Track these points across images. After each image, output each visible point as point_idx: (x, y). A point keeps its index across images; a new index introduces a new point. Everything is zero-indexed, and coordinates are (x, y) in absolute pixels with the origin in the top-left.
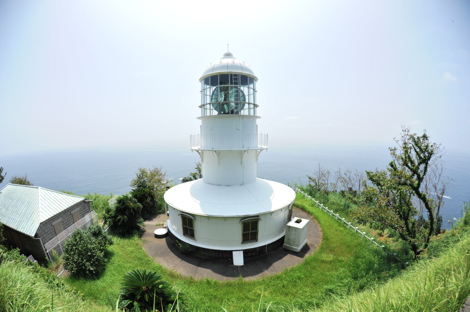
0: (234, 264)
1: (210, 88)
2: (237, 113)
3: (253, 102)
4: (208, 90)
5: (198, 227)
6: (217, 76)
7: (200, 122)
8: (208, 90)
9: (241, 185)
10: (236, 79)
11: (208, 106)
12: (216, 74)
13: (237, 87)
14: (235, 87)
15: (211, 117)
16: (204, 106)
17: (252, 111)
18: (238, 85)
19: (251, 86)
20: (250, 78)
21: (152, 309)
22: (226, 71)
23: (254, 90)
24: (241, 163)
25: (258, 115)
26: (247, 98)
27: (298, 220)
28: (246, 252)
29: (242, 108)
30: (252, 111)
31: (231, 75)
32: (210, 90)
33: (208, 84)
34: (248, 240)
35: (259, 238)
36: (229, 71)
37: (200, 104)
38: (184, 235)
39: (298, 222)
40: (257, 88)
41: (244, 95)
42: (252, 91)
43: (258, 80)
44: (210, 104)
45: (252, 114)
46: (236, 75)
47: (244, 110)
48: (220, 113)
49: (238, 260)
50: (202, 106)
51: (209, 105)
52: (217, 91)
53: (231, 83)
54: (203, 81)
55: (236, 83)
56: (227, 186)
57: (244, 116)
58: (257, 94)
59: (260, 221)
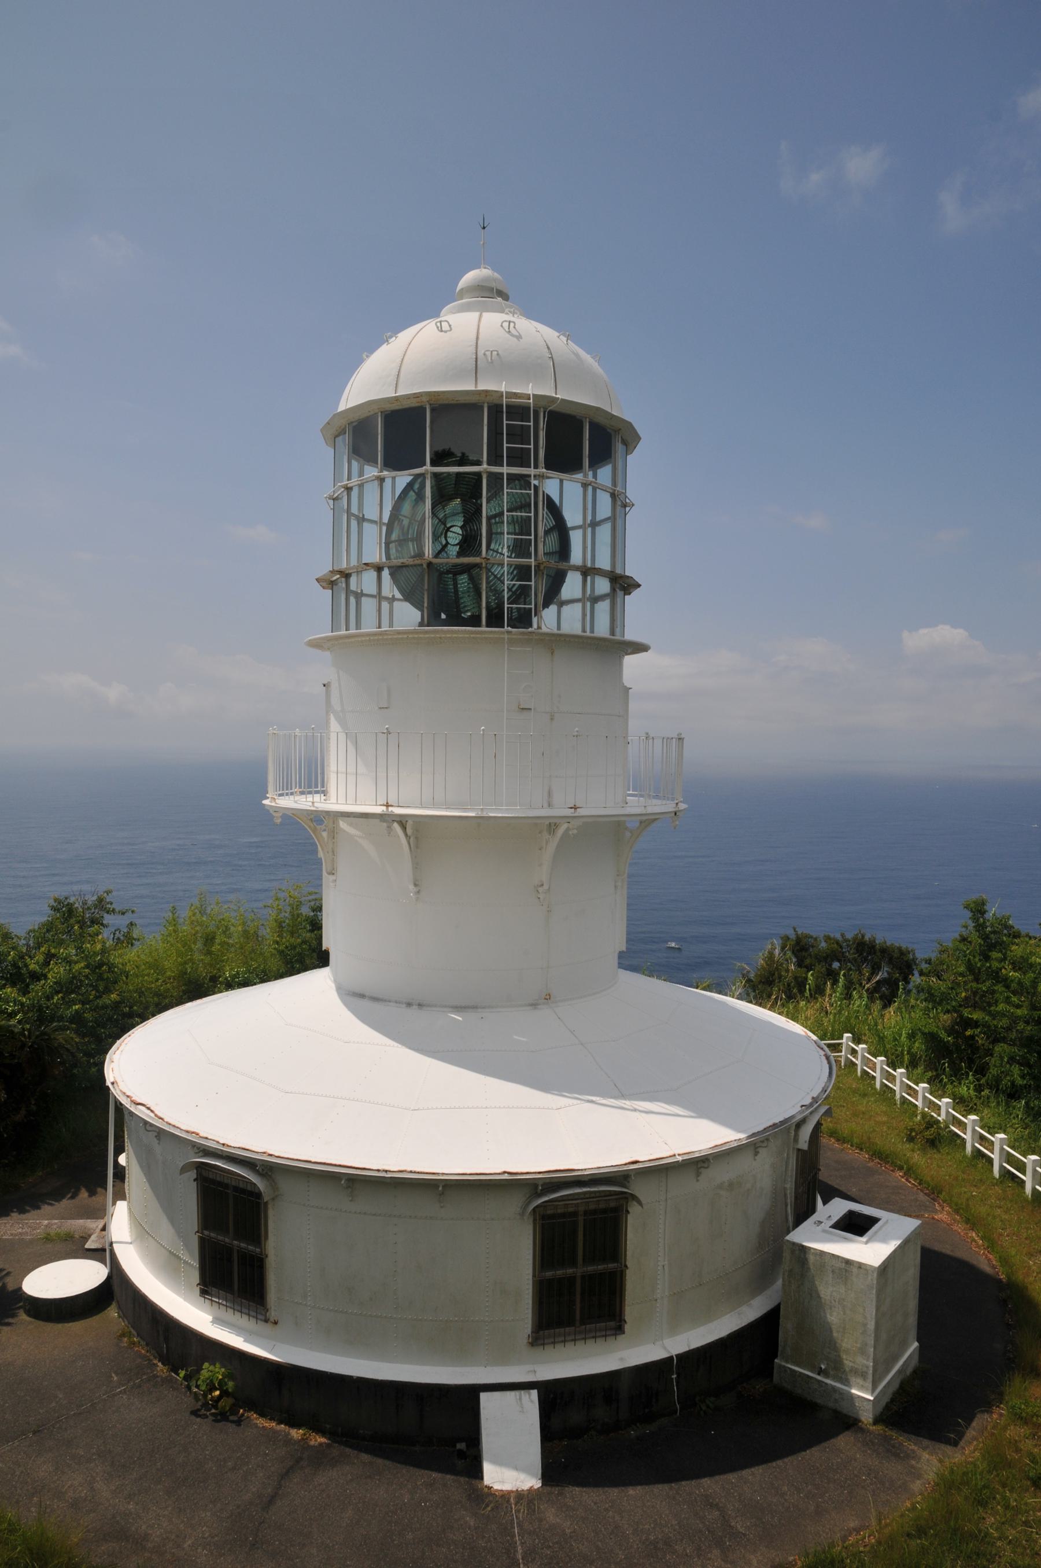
1: (382, 480)
2: (523, 620)
4: (372, 492)
5: (290, 1241)
8: (372, 492)
10: (519, 435)
11: (368, 581)
12: (414, 403)
13: (523, 481)
14: (512, 478)
16: (347, 576)
18: (531, 471)
19: (604, 474)
20: (595, 427)
21: (104, 1186)
22: (470, 387)
23: (613, 496)
26: (576, 539)
27: (851, 1214)
28: (556, 1399)
29: (552, 595)
31: (496, 410)
32: (382, 489)
33: (372, 460)
34: (570, 1323)
35: (630, 1312)
36: (481, 387)
37: (324, 567)
38: (204, 1293)
39: (856, 1225)
41: (561, 529)
42: (604, 507)
43: (637, 438)
44: (379, 569)
46: (519, 411)
47: (562, 604)
48: (432, 618)
50: (337, 580)
51: (372, 574)
52: (420, 497)
53: (495, 458)
54: (344, 443)
55: (519, 458)
59: (634, 1209)
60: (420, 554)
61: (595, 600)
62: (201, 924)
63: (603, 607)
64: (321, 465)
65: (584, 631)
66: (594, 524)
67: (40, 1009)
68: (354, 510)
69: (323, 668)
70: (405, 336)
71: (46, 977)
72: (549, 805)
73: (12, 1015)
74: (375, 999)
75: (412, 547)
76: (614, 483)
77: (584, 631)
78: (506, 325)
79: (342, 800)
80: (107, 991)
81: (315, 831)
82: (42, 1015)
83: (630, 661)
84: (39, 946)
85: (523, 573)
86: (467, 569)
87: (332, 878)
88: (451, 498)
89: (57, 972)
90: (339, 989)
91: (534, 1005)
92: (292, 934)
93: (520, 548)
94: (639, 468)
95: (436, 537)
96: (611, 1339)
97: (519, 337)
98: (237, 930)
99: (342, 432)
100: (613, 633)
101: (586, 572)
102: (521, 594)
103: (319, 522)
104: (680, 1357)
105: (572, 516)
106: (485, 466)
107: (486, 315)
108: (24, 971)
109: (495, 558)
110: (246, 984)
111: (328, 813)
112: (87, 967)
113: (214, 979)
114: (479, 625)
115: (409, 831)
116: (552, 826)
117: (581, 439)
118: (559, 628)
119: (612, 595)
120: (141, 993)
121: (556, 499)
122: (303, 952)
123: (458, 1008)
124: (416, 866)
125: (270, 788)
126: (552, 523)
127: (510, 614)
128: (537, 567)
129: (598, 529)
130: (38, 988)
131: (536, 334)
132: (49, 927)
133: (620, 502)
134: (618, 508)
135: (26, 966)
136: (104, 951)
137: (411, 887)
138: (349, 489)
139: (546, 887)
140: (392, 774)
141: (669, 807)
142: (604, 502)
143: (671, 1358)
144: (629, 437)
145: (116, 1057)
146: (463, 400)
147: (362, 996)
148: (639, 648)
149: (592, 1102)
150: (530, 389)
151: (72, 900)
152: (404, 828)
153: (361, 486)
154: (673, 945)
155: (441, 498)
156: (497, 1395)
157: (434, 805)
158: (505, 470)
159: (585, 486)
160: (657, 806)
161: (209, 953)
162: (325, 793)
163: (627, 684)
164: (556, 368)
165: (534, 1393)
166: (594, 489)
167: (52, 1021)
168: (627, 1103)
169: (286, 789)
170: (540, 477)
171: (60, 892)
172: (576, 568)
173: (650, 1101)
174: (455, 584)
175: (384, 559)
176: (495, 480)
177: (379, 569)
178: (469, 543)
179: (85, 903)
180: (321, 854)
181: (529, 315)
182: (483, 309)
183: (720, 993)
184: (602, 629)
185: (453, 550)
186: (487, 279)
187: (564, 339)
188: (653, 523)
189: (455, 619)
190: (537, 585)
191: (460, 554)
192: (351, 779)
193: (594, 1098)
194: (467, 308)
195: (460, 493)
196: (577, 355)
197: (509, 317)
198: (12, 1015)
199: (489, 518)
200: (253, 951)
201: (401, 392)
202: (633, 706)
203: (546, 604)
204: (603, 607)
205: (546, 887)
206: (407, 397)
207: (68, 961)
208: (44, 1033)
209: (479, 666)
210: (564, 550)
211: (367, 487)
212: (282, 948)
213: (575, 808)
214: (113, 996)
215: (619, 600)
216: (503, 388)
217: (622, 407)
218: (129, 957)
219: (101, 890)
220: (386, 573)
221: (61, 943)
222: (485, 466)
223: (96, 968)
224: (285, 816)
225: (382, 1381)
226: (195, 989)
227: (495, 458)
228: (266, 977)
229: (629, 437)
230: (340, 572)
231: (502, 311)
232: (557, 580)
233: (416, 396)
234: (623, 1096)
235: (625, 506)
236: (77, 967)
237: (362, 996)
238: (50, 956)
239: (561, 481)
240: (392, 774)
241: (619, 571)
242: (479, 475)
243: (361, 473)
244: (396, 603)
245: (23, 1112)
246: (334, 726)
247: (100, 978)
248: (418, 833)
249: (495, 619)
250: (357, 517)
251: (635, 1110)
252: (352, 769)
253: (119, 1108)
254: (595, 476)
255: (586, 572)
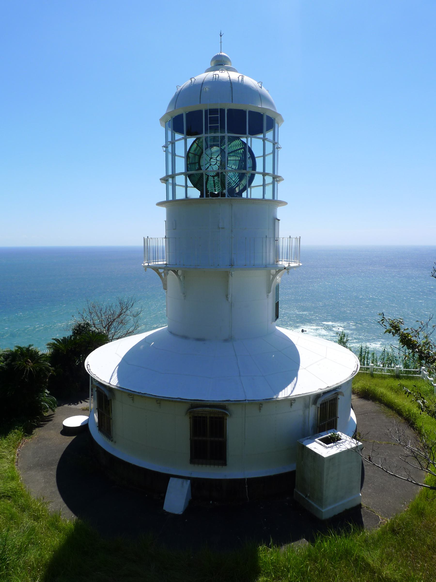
0: (164, 508)
3: (271, 172)
6: (201, 111)
7: (163, 212)
9: (226, 340)
15: (187, 200)
17: (269, 189)
19: (269, 135)
20: (268, 117)
24: (227, 296)
25: (280, 197)
28: (197, 484)
30: (269, 189)
32: (183, 144)
33: (181, 132)
37: (164, 175)
40: (281, 142)
42: (269, 147)
45: (269, 196)
49: (176, 499)
56: (198, 340)
57: (244, 199)
58: (281, 153)
96: (220, 467)
104: (249, 479)
119: (273, 183)
143: (244, 479)
156: (176, 479)
165: (189, 481)
225: (75, 416)
255: (264, 174)
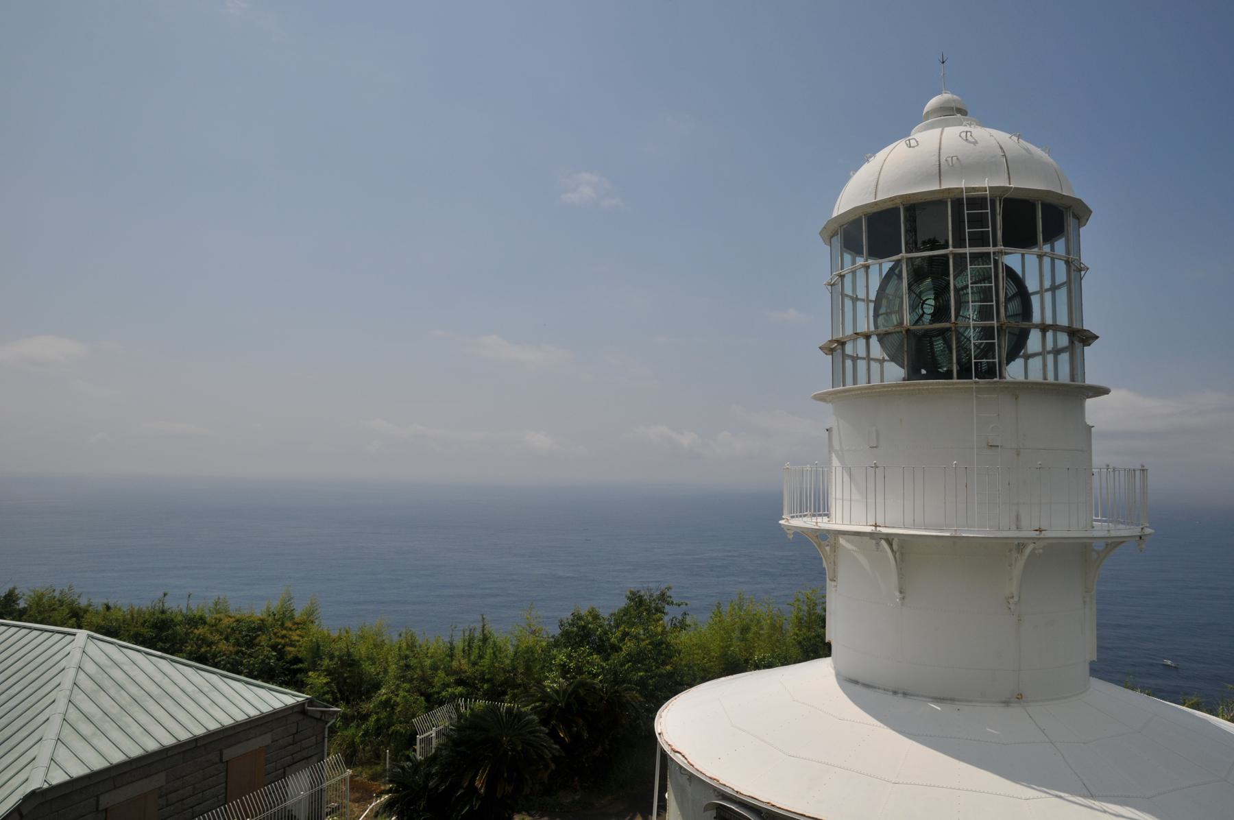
1: (867, 267)
14: (975, 257)
16: (842, 344)
18: (991, 249)
19: (1060, 245)
22: (936, 187)
23: (1068, 262)
26: (1035, 301)
31: (958, 203)
33: (860, 253)
36: (944, 187)
41: (1023, 295)
46: (977, 201)
47: (1027, 357)
48: (913, 374)
50: (835, 348)
53: (959, 242)
54: (837, 241)
55: (981, 240)
60: (901, 323)
61: (1057, 352)
62: (739, 617)
63: (1064, 358)
64: (820, 258)
65: (1045, 378)
66: (1054, 288)
67: (615, 673)
68: (848, 291)
69: (828, 415)
70: (881, 155)
71: (621, 649)
72: (1018, 528)
73: (595, 676)
74: (866, 685)
75: (894, 319)
76: (1068, 252)
77: (1045, 378)
78: (963, 135)
79: (847, 521)
80: (664, 663)
81: (820, 546)
82: (616, 678)
83: (1090, 403)
84: (617, 626)
85: (987, 332)
86: (943, 333)
87: (833, 584)
88: (925, 278)
89: (628, 646)
90: (838, 675)
91: (1007, 703)
92: (809, 629)
93: (985, 313)
94: (1092, 240)
95: (913, 308)
97: (975, 143)
98: (766, 623)
99: (835, 234)
100: (1073, 379)
101: (1044, 329)
102: (987, 351)
103: (816, 303)
105: (1032, 285)
106: (951, 249)
107: (948, 130)
108: (607, 644)
109: (961, 322)
110: (770, 666)
111: (828, 531)
112: (650, 644)
113: (746, 661)
114: (951, 378)
115: (895, 547)
116: (1020, 546)
117: (1036, 218)
118: (1026, 376)
119: (1070, 348)
120: (690, 668)
121: (1018, 271)
122: (816, 647)
123: (939, 700)
124: (901, 575)
125: (786, 511)
126: (1013, 290)
127: (981, 367)
128: (1000, 328)
129: (1057, 292)
130: (615, 658)
131: (989, 138)
132: (626, 611)
133: (1075, 268)
134: (1073, 273)
135: (609, 640)
136: (664, 633)
137: (897, 593)
138: (842, 277)
139: (1016, 599)
140: (880, 500)
141: (1136, 531)
142: (1061, 267)
144: (1081, 212)
145: (664, 714)
146: (929, 198)
147: (856, 682)
148: (1100, 391)
149: (1060, 797)
150: (986, 183)
151: (642, 593)
152: (890, 545)
153: (854, 272)
154: (1169, 662)
155: (917, 275)
157: (914, 527)
158: (967, 250)
159: (1040, 257)
160: (1122, 531)
161: (744, 640)
162: (828, 515)
163: (1089, 422)
164: (1008, 163)
166: (1053, 260)
167: (624, 682)
168: (1097, 804)
169: (801, 511)
170: (1002, 253)
171: (633, 586)
172: (1036, 326)
173: (1121, 805)
174: (932, 346)
175: (872, 328)
176: (960, 259)
177: (867, 337)
178: (941, 312)
179: (651, 596)
180: (825, 565)
181: (984, 123)
182: (944, 125)
183: (1211, 712)
184: (1064, 377)
185: (927, 318)
186: (948, 101)
187: (1015, 138)
188: (1111, 280)
189: (934, 374)
190: (1002, 345)
191: (932, 321)
192: (847, 503)
193: (1062, 794)
194: (932, 126)
195: (931, 274)
196: (1027, 150)
197: (967, 128)
198: (595, 676)
199: (957, 290)
200: (778, 641)
201: (880, 197)
202: (1096, 445)
203: (1011, 358)
204: (1064, 358)
205: (1016, 599)
206: (884, 201)
207: (636, 637)
208: (616, 692)
209: (954, 408)
210: (1026, 312)
211: (858, 273)
212: (800, 638)
213: (1040, 530)
214: (668, 667)
215: (1078, 351)
216: (963, 184)
217: (1073, 189)
218: (683, 639)
219: (663, 586)
220: (874, 340)
221: (633, 625)
222: (951, 249)
223: (657, 645)
224: (795, 534)
226: (732, 666)
227: (959, 242)
228: (786, 661)
229: (1081, 212)
230: (837, 341)
231: (961, 124)
232: (1022, 337)
233: (891, 199)
234: (1092, 796)
235: (1080, 270)
236: (643, 644)
237: (856, 682)
238: (625, 634)
239: (1023, 255)
240: (880, 500)
241: (1076, 326)
242: (946, 256)
243: (854, 262)
244: (886, 364)
245: (600, 749)
246: (835, 462)
247: (660, 653)
248: (903, 550)
249: (964, 373)
250: (852, 298)
251: (1105, 812)
252: (847, 496)
253: (664, 755)
254: (1053, 249)
255: (1044, 329)
